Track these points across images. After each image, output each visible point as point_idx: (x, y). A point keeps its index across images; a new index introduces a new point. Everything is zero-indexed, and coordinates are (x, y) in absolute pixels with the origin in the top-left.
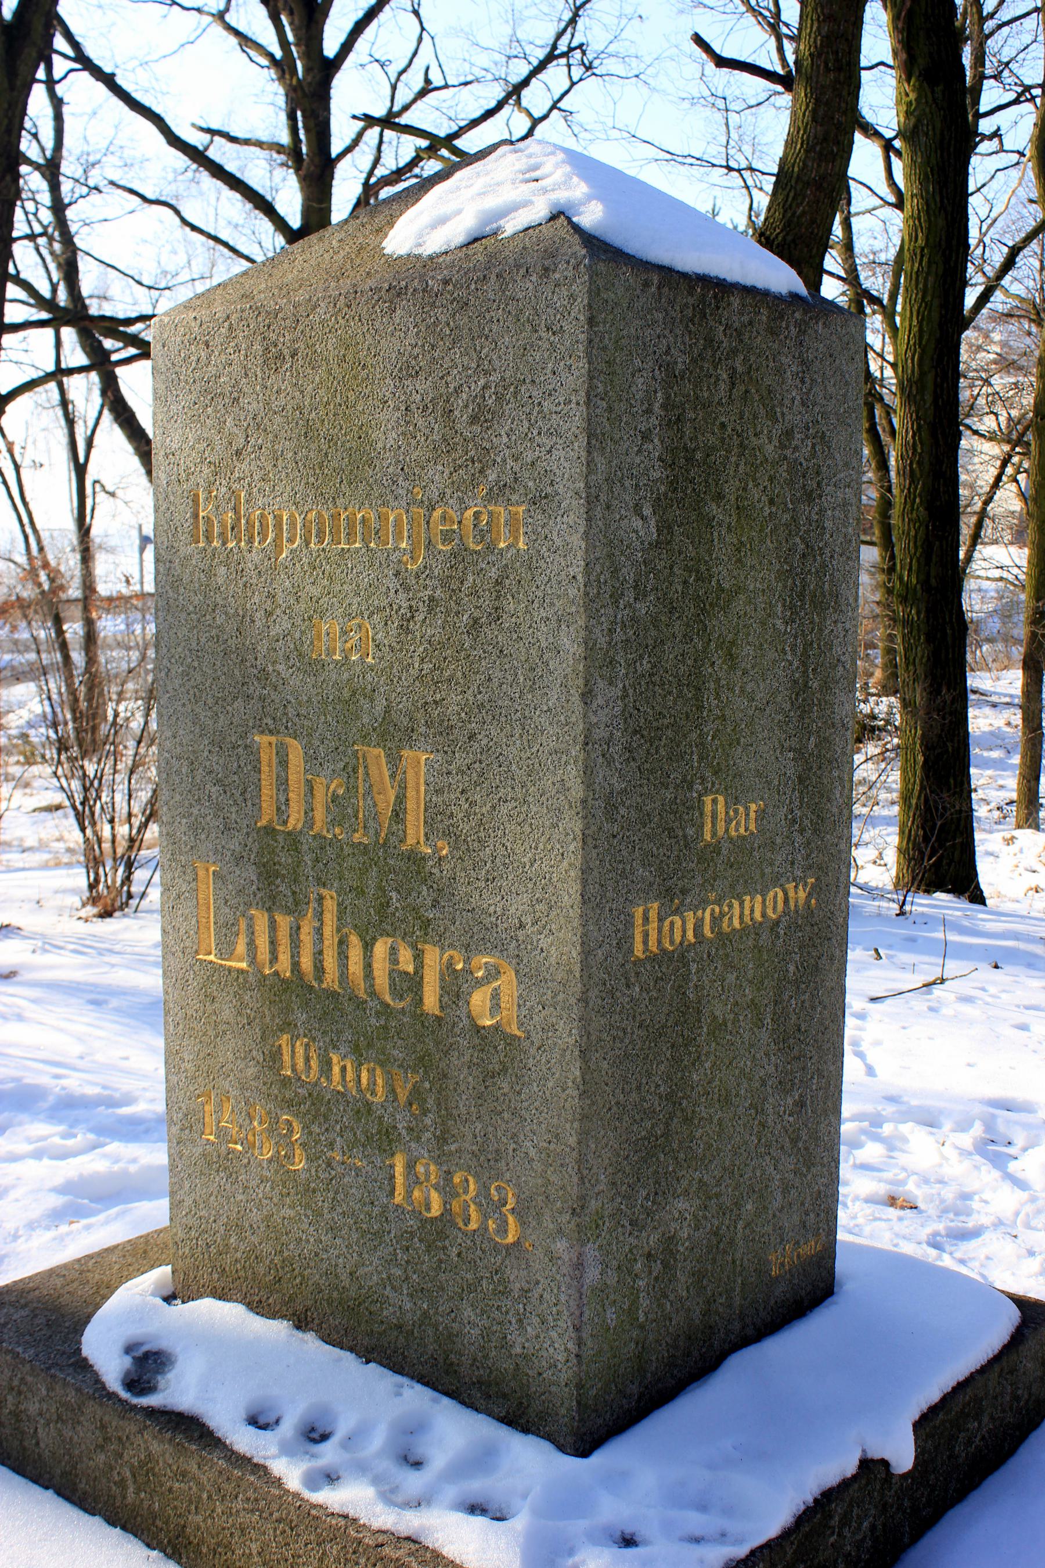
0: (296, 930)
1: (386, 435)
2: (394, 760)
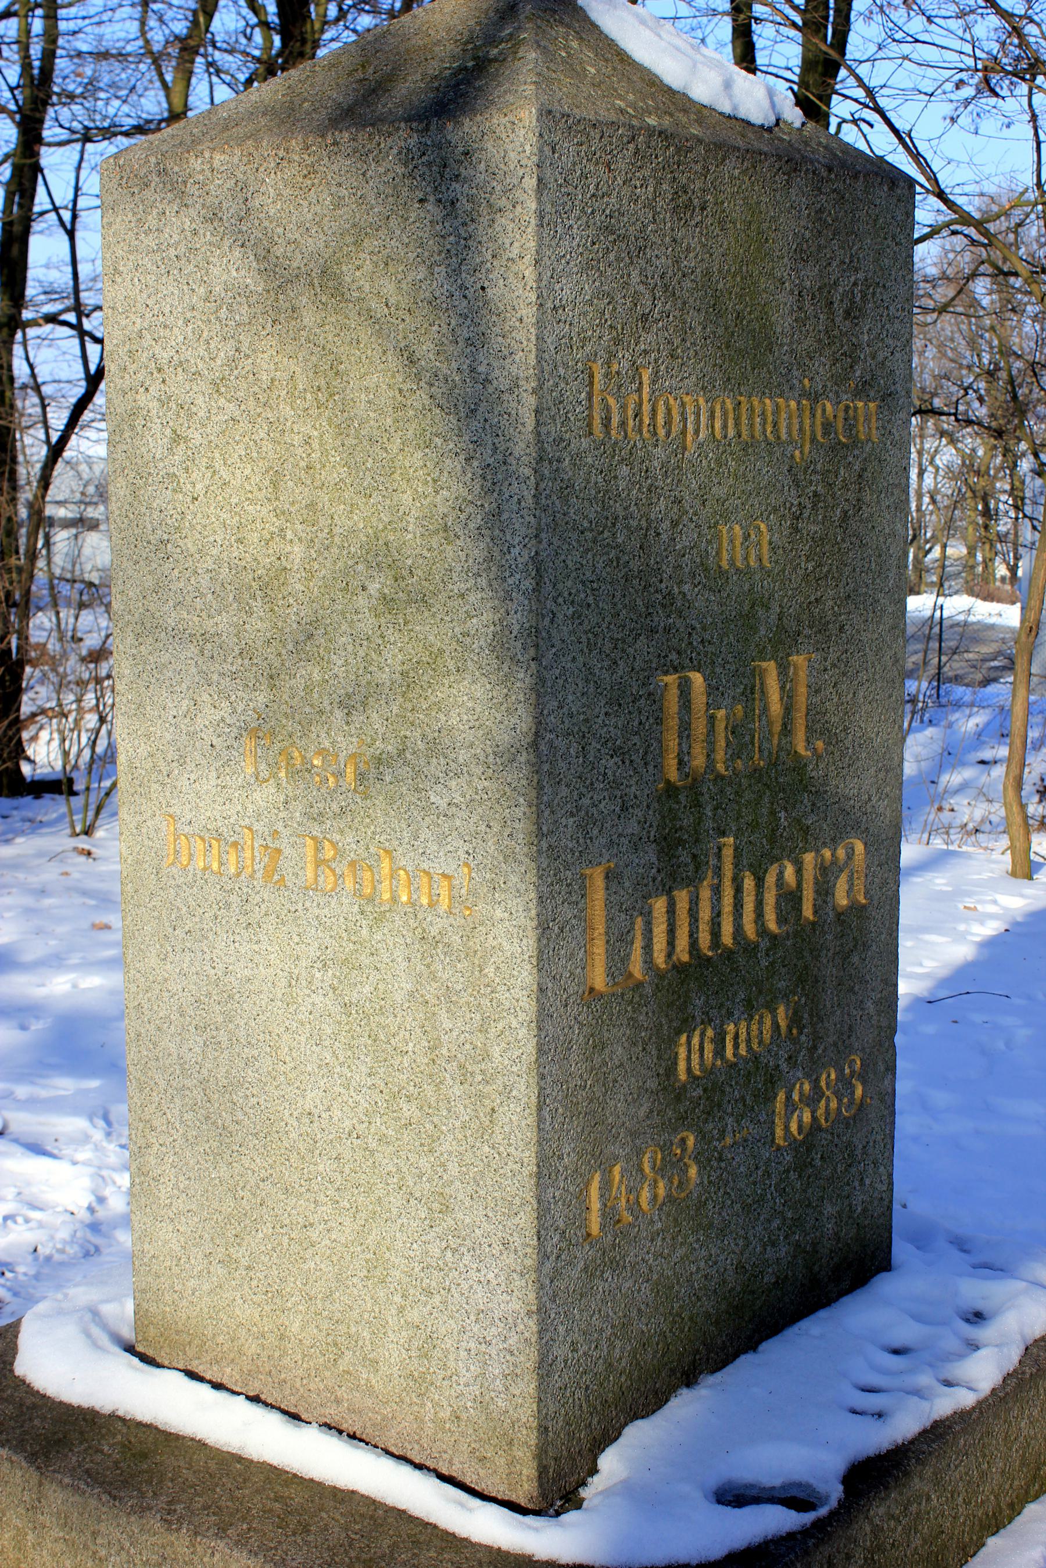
1: (782, 321)
2: (783, 668)
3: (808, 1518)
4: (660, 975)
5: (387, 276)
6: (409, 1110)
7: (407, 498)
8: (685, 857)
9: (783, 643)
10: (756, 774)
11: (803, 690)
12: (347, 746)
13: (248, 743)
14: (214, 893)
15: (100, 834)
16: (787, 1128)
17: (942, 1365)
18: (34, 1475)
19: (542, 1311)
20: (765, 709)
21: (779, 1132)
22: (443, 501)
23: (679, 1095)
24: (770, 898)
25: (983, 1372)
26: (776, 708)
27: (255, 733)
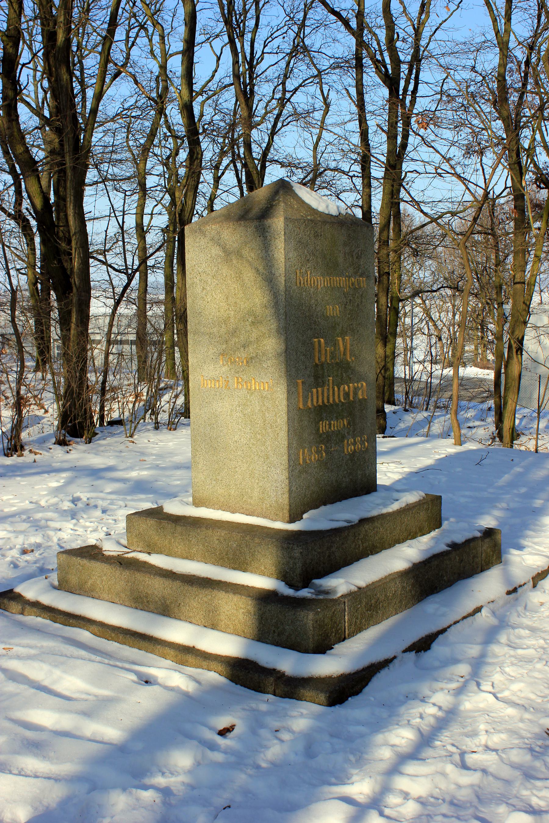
0: (323, 392)
1: (341, 260)
2: (343, 339)
3: (349, 524)
4: (315, 407)
5: (251, 253)
6: (259, 437)
7: (257, 300)
8: (320, 381)
9: (343, 334)
10: (337, 364)
11: (348, 345)
12: (244, 355)
13: (221, 357)
14: (213, 392)
15: (135, 437)
16: (347, 450)
17: (385, 505)
18: (174, 525)
19: (289, 478)
20: (339, 349)
21: (346, 450)
22: (265, 300)
23: (321, 436)
24: (342, 394)
25: (395, 507)
26: (342, 349)
27: (223, 355)
